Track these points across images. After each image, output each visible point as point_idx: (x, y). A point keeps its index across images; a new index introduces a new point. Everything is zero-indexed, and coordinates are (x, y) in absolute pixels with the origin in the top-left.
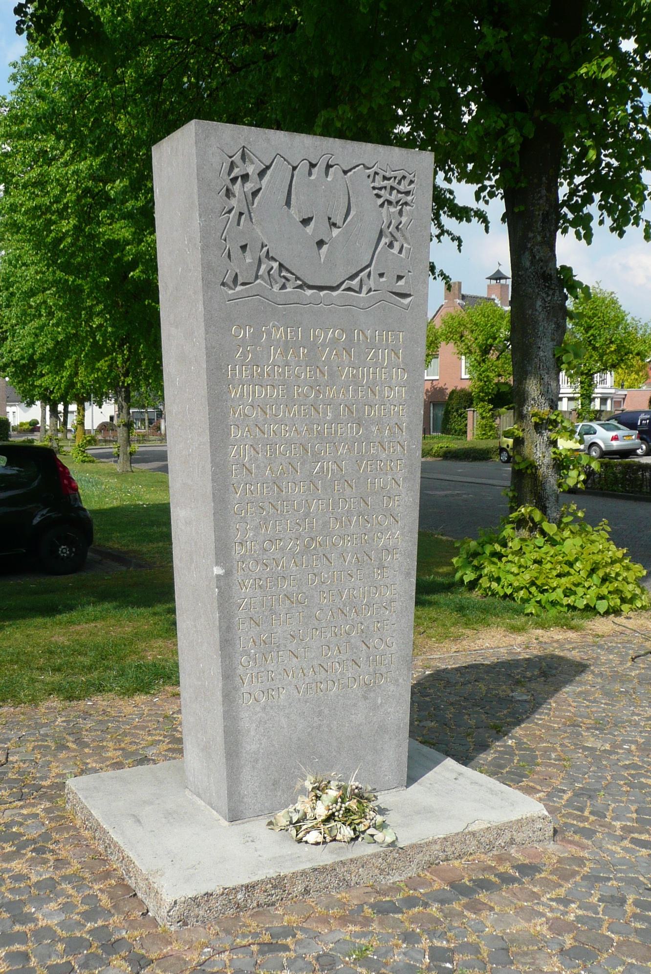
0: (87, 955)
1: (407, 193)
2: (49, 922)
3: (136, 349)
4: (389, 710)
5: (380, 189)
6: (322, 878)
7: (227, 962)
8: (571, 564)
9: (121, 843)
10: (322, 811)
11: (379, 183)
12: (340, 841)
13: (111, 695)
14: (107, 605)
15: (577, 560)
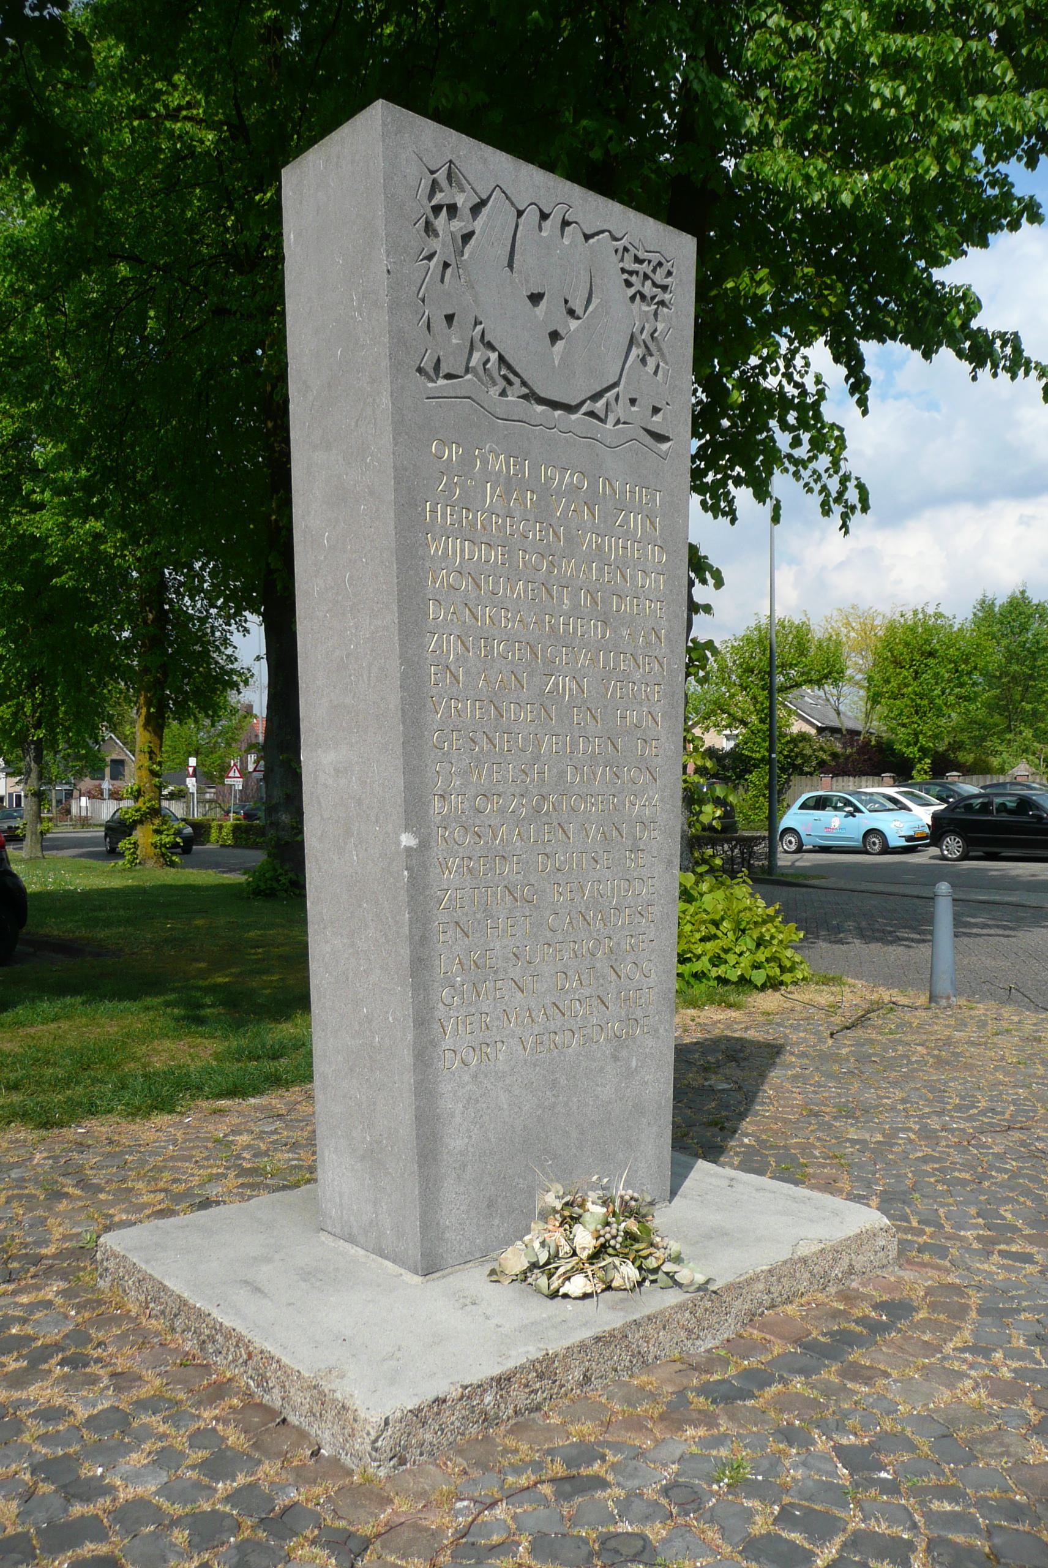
0: (239, 1547)
1: (664, 288)
2: (140, 1490)
6: (606, 1353)
7: (510, 1522)
8: (716, 924)
9: (241, 1328)
10: (585, 1239)
12: (618, 1289)
13: (113, 1118)
14: (68, 1000)
15: (723, 919)
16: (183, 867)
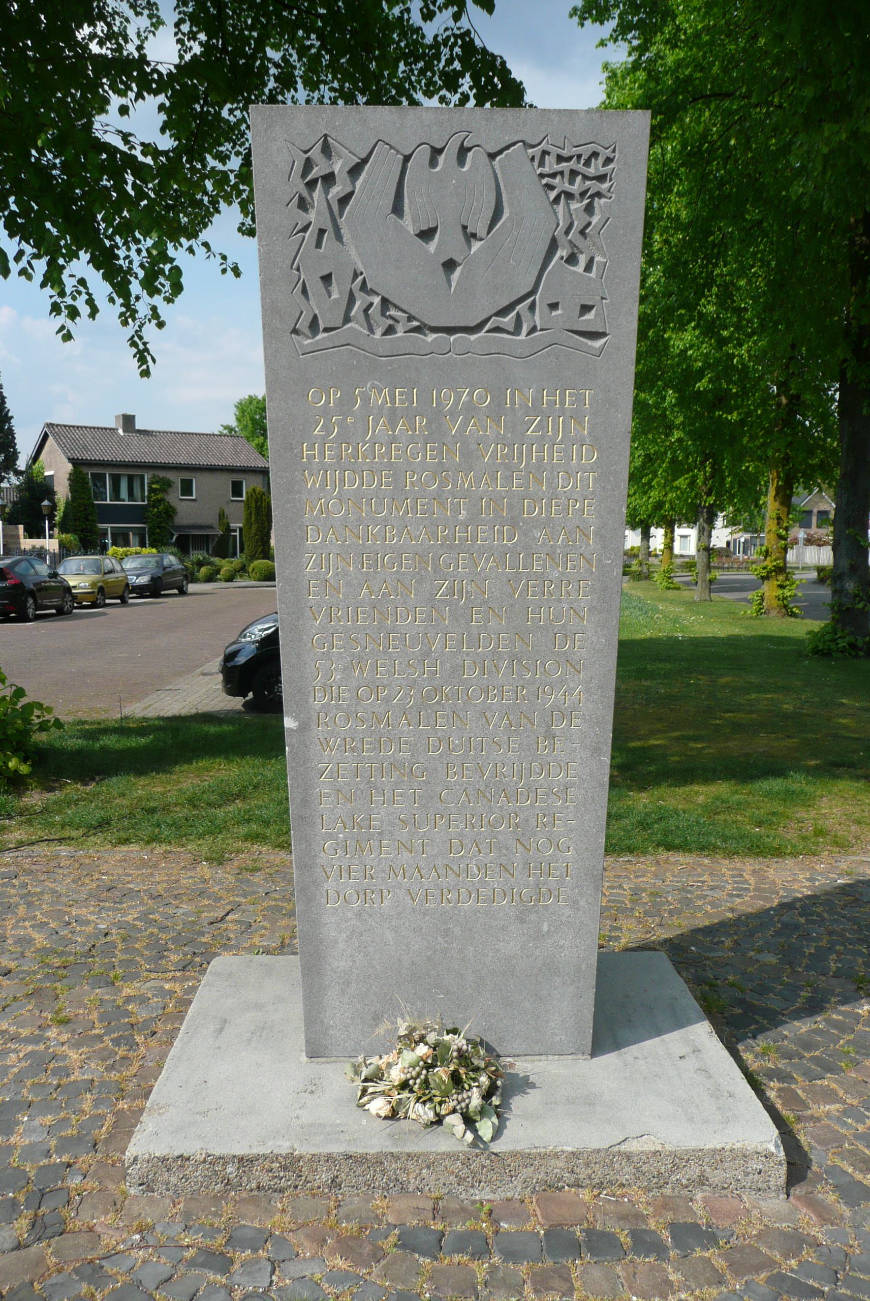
1: (602, 178)
3: (721, 465)
4: (561, 943)
5: (553, 175)
11: (551, 165)
16: (803, 618)
